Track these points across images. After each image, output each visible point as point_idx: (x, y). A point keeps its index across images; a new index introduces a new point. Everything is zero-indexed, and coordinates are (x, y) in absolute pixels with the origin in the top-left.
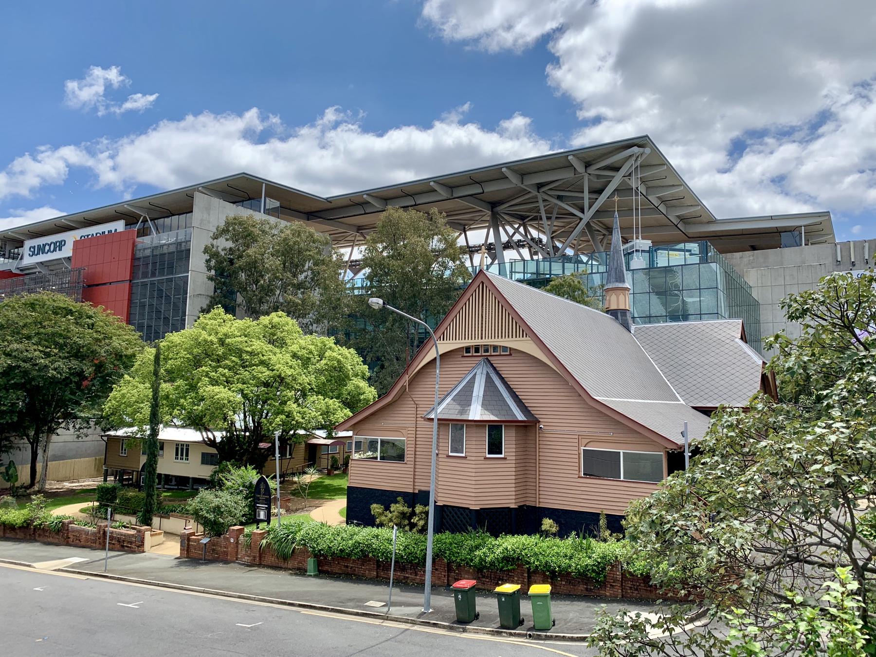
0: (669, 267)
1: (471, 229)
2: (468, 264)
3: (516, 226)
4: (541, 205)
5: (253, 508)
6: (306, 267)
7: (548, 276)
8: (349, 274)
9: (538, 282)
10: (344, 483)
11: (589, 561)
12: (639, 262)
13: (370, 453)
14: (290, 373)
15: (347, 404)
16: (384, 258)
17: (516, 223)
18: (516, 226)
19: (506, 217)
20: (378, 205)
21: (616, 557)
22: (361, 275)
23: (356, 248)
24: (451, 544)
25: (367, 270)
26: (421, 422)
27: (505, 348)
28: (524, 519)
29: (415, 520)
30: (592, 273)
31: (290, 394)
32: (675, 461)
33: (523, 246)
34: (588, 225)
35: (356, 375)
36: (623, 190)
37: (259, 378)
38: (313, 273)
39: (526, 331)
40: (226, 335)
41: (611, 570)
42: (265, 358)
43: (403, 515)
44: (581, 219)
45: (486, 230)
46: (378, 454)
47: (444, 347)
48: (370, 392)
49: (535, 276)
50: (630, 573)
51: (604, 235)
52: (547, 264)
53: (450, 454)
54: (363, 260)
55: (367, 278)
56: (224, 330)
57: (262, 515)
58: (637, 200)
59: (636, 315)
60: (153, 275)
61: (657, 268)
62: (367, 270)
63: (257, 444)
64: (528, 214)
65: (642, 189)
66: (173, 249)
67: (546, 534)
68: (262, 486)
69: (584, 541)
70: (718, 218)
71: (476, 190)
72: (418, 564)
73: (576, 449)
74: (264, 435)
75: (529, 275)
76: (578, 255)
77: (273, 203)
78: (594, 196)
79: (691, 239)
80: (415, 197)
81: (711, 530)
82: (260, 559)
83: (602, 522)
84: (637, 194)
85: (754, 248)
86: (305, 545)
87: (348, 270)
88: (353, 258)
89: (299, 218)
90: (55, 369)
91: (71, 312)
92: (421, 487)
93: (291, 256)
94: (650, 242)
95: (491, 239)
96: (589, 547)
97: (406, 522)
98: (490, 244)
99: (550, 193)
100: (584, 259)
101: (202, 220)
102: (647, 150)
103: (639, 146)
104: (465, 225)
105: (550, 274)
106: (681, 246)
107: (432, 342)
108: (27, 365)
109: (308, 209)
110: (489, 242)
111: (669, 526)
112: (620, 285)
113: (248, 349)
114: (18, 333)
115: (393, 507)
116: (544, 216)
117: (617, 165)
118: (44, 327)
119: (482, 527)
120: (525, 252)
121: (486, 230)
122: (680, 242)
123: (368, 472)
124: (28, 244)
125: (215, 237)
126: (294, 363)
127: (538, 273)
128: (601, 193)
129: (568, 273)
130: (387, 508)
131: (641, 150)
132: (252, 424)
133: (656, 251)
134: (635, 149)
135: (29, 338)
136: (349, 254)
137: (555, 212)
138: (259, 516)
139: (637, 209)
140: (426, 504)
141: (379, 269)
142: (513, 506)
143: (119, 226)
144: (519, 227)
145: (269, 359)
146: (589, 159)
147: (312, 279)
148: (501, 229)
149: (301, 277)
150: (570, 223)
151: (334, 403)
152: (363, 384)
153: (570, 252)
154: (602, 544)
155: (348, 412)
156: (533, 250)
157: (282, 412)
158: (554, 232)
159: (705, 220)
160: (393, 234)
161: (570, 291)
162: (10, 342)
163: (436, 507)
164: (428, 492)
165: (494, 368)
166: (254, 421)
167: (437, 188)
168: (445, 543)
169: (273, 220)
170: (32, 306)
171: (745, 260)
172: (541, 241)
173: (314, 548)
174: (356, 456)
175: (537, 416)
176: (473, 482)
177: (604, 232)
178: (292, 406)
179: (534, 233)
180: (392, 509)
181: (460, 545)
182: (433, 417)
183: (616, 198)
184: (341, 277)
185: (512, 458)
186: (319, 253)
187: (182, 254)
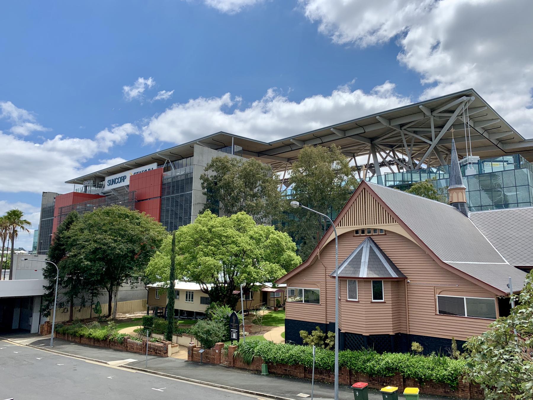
2: (357, 177)
3: (388, 152)
5: (229, 332)
7: (410, 182)
8: (284, 187)
9: (404, 186)
13: (298, 298)
14: (249, 248)
15: (284, 266)
17: (387, 150)
20: (299, 145)
22: (290, 188)
24: (351, 358)
25: (294, 185)
26: (329, 279)
29: (327, 341)
30: (440, 179)
31: (249, 261)
33: (393, 164)
34: (435, 148)
35: (289, 249)
36: (458, 125)
39: (395, 218)
40: (212, 227)
42: (234, 239)
44: (430, 145)
45: (368, 155)
46: (303, 299)
47: (340, 230)
48: (297, 259)
49: (401, 183)
51: (447, 154)
52: (409, 175)
53: (348, 300)
56: (211, 223)
57: (234, 336)
58: (467, 131)
60: (173, 193)
61: (484, 174)
62: (294, 185)
65: (471, 123)
66: (183, 178)
68: (234, 318)
69: (441, 359)
71: (361, 131)
73: (433, 296)
75: (398, 182)
77: (238, 148)
78: (438, 130)
79: (507, 153)
80: (322, 138)
82: (234, 364)
84: (467, 127)
90: (120, 249)
91: (127, 216)
93: (249, 179)
94: (478, 157)
96: (445, 363)
97: (322, 342)
98: (371, 164)
99: (409, 129)
100: (435, 170)
101: (199, 161)
102: (473, 98)
103: (467, 96)
105: (412, 181)
106: (501, 158)
107: (332, 229)
108: (105, 247)
111: (496, 358)
112: (459, 186)
113: (225, 234)
114: (100, 229)
115: (314, 333)
118: (114, 225)
120: (395, 168)
121: (368, 155)
122: (500, 156)
124: (107, 179)
125: (206, 170)
126: (251, 242)
127: (403, 181)
129: (423, 180)
130: (310, 333)
131: (468, 98)
133: (483, 163)
134: (464, 98)
135: (106, 232)
138: (233, 336)
140: (334, 332)
141: (300, 183)
143: (154, 166)
145: (237, 240)
148: (377, 154)
151: (276, 266)
152: (293, 254)
153: (424, 166)
155: (284, 272)
162: (96, 234)
163: (340, 333)
164: (334, 324)
165: (375, 244)
166: (229, 277)
168: (347, 357)
169: (238, 158)
170: (107, 213)
172: (404, 160)
173: (265, 357)
174: (289, 300)
176: (364, 318)
178: (251, 268)
179: (400, 156)
180: (313, 334)
181: (357, 358)
183: (452, 130)
184: (279, 190)
187: (188, 180)
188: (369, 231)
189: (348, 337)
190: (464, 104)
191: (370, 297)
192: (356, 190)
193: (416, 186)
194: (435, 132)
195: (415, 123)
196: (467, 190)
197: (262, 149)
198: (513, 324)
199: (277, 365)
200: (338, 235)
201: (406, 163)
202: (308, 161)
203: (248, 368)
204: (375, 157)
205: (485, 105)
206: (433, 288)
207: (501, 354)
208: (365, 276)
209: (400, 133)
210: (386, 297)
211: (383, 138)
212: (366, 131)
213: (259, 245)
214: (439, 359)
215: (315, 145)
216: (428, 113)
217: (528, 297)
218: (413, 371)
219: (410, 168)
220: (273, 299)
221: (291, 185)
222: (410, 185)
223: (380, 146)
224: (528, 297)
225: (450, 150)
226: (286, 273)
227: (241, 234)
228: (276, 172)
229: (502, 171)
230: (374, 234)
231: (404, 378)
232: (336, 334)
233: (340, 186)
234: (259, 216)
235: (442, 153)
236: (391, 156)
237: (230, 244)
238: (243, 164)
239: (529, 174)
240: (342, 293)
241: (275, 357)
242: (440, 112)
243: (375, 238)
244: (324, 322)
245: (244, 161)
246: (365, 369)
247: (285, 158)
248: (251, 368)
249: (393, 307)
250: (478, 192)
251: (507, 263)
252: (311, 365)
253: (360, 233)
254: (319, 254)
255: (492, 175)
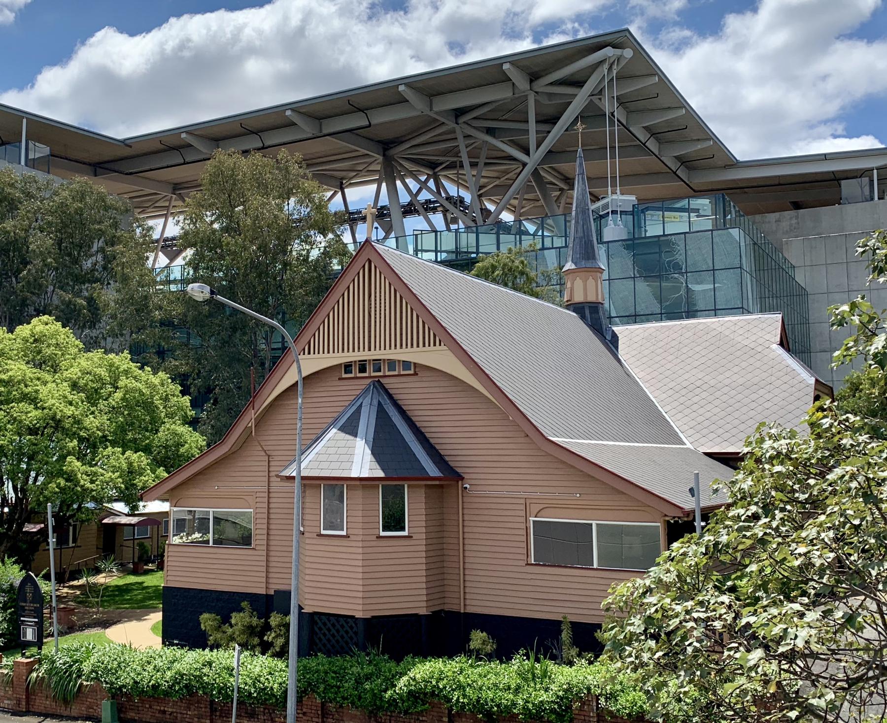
0: (664, 235)
1: (351, 185)
2: (347, 238)
4: (461, 143)
5: (15, 625)
6: (95, 248)
7: (473, 255)
8: (163, 260)
9: (461, 262)
10: (155, 580)
11: (544, 697)
12: (614, 230)
13: (197, 535)
14: (69, 413)
15: (160, 461)
16: (214, 231)
17: (423, 173)
18: (423, 178)
19: (407, 165)
20: (203, 148)
21: (589, 689)
22: (179, 261)
23: (170, 219)
24: (326, 673)
25: (189, 253)
26: (276, 483)
27: (406, 365)
28: (442, 631)
29: (269, 637)
30: (543, 248)
31: (71, 445)
32: (679, 528)
33: (434, 210)
34: (536, 173)
35: (170, 416)
36: (592, 115)
37: (21, 422)
38: (105, 258)
39: (440, 335)
41: (581, 709)
42: (30, 389)
43: (250, 630)
44: (524, 165)
45: (374, 186)
46: (210, 536)
47: (310, 364)
48: (194, 440)
49: (453, 256)
50: (611, 713)
51: (561, 190)
52: (473, 236)
54: (181, 237)
55: (189, 264)
57: (30, 635)
58: (612, 134)
59: (613, 314)
61: (646, 238)
62: (189, 253)
63: (20, 526)
64: (442, 159)
65: (620, 114)
67: (478, 656)
68: (29, 588)
69: (537, 665)
70: (740, 158)
71: (358, 121)
72: (276, 704)
74: (33, 511)
75: (444, 255)
76: (520, 221)
77: (41, 150)
78: (544, 127)
79: (698, 193)
80: (264, 135)
81: (752, 619)
82: (28, 703)
83: (566, 635)
84: (612, 123)
85: (797, 206)
86: (97, 678)
87: (160, 253)
88: (168, 234)
89: (82, 173)
92: (277, 585)
93: (74, 233)
94: (633, 198)
95: (384, 200)
96: (545, 674)
97: (256, 640)
98: (383, 207)
99: (477, 123)
100: (531, 228)
102: (628, 53)
103: (614, 47)
104: (342, 179)
105: (477, 253)
106: (684, 203)
107: (289, 359)
109: (96, 159)
110: (380, 204)
111: (677, 621)
115: (235, 618)
116: (466, 162)
117: (579, 82)
119: (375, 644)
120: (438, 219)
121: (374, 186)
122: (681, 198)
123: (190, 565)
126: (75, 397)
127: (457, 252)
128: (555, 123)
129: (504, 249)
130: (226, 620)
131: (618, 52)
132: (12, 494)
133: (643, 211)
134: (608, 51)
136: (160, 228)
137: (484, 154)
138: (25, 635)
139: (613, 148)
140: (287, 613)
141: (205, 246)
142: (423, 612)
144: (427, 180)
145: (37, 391)
146: (536, 69)
147: (105, 268)
149: (88, 264)
150: (506, 172)
151: (139, 459)
152: (184, 430)
153: (507, 217)
154: (566, 669)
155: (162, 472)
156: (449, 216)
157: (61, 473)
158: (481, 188)
159: (720, 163)
160: (227, 191)
161: (513, 277)
163: (301, 615)
164: (289, 593)
165: (390, 397)
166: (15, 488)
167: (296, 118)
168: (317, 671)
169: (40, 176)
171: (785, 225)
172: (462, 200)
173: (112, 683)
174: (176, 540)
175: (459, 470)
177: (562, 185)
178: (74, 464)
179: (452, 190)
180: (233, 621)
181: (341, 676)
182: (294, 474)
183: (580, 127)
184: (150, 263)
185: (421, 536)
186: (115, 225)
188: (377, 364)
189: (320, 624)
190: (606, 66)
191: (375, 525)
192: (344, 271)
193: (486, 263)
194: (537, 132)
195: (494, 105)
196: (605, 276)
197: (108, 154)
198: (717, 544)
199: (142, 701)
200: (304, 374)
201: (466, 208)
202: (227, 191)
203: (65, 713)
204: (393, 191)
205: (654, 70)
206: (523, 501)
207: (688, 612)
208: (365, 474)
209: (453, 131)
210: (413, 524)
211: (407, 145)
212: (372, 123)
213: (94, 404)
214: (533, 666)
215: (245, 152)
216: (521, 82)
217: (750, 483)
218: (474, 697)
219: (474, 221)
220: (130, 543)
221: (184, 254)
222: (473, 262)
223: (403, 163)
224: (750, 483)
225: (569, 182)
226: (166, 475)
227: (48, 377)
228: (145, 219)
229: (685, 233)
230: (387, 373)
231: (450, 715)
232: (293, 619)
233: (306, 259)
234: (94, 333)
235: (547, 190)
236: (429, 190)
237: (20, 400)
238: (56, 193)
239: (743, 244)
240: (307, 517)
241: (136, 682)
242: (551, 84)
243: (391, 384)
244: (263, 591)
245: (63, 187)
246: (360, 698)
247: (167, 183)
248: (74, 713)
249: (431, 547)
250: (631, 282)
251: (689, 445)
252: (228, 697)
253: (356, 372)
254: (252, 424)
255: (663, 242)
